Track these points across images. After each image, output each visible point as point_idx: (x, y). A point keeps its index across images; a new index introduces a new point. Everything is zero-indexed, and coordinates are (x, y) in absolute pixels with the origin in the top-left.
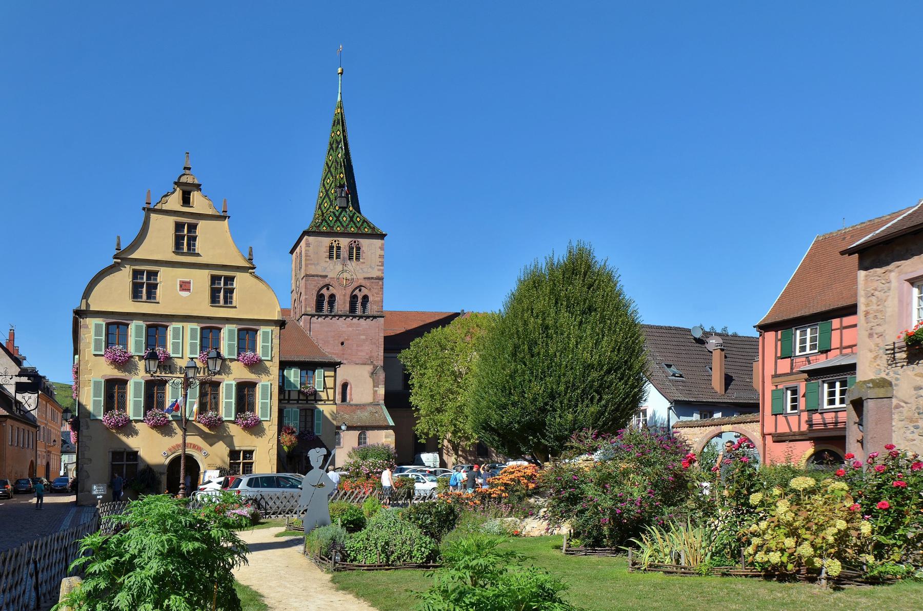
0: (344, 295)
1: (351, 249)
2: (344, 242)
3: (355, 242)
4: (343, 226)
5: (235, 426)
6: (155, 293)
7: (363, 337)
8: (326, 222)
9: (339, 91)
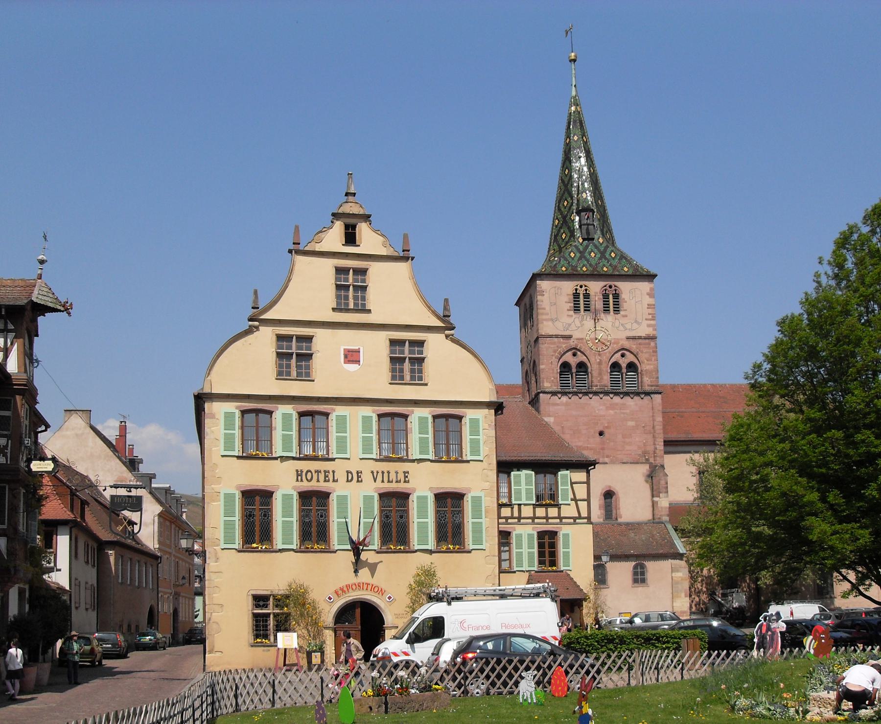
0: (600, 363)
1: (606, 296)
2: (595, 287)
7: (631, 424)
8: (566, 259)
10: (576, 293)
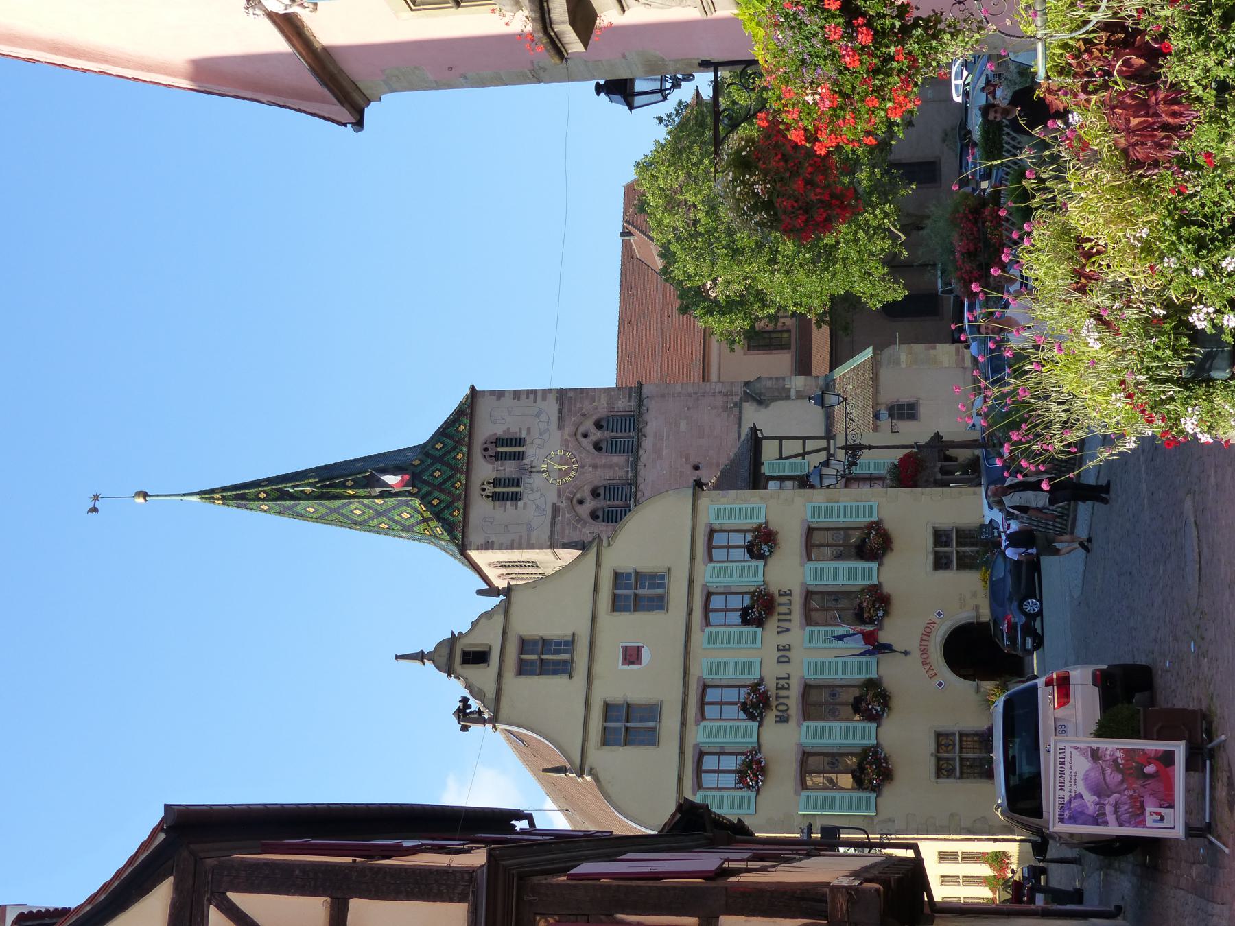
0: (595, 467)
1: (499, 457)
2: (484, 471)
7: (683, 425)
10: (492, 497)
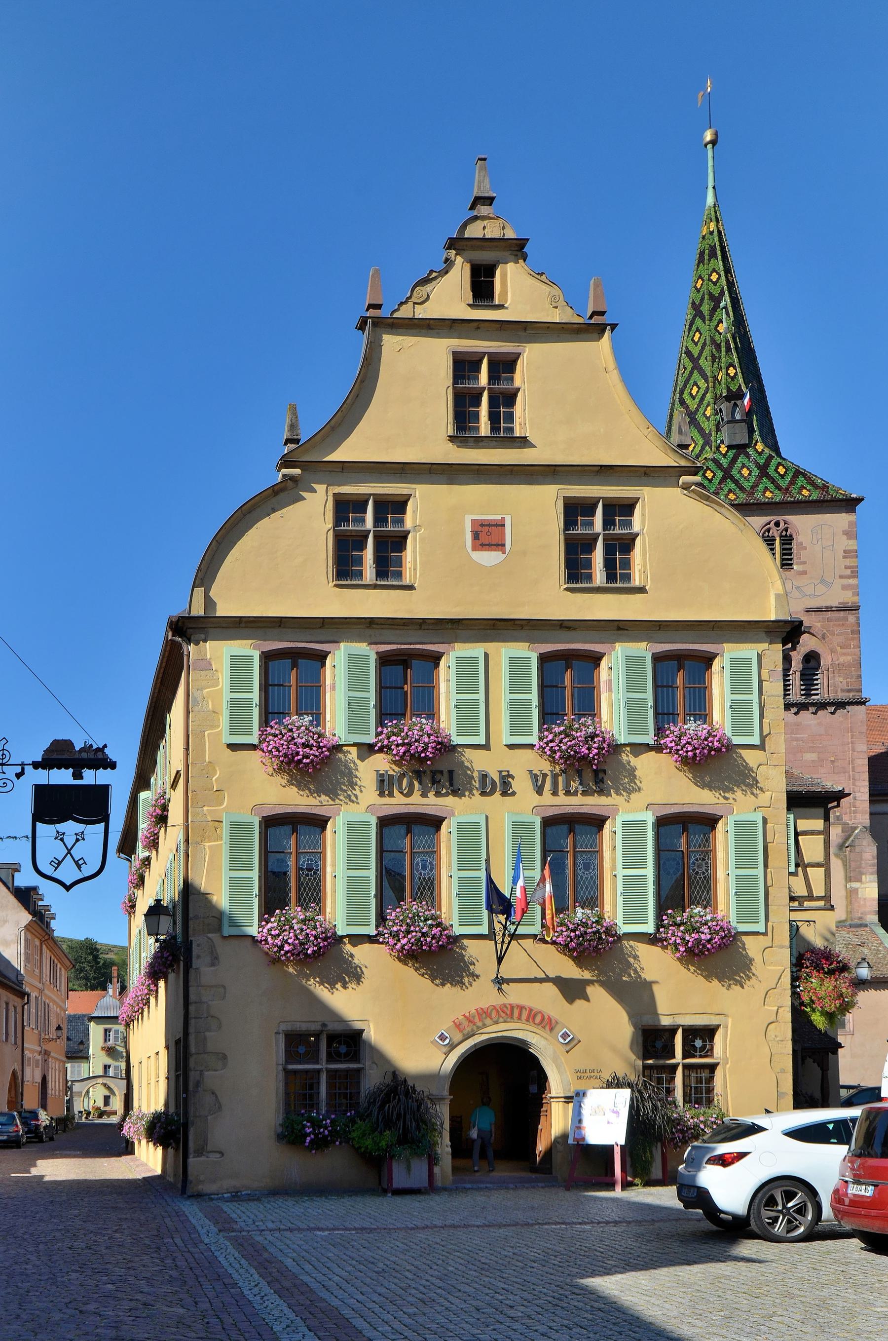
3: (777, 524)
4: (742, 489)
5: (656, 950)
6: (399, 562)
9: (711, 183)
